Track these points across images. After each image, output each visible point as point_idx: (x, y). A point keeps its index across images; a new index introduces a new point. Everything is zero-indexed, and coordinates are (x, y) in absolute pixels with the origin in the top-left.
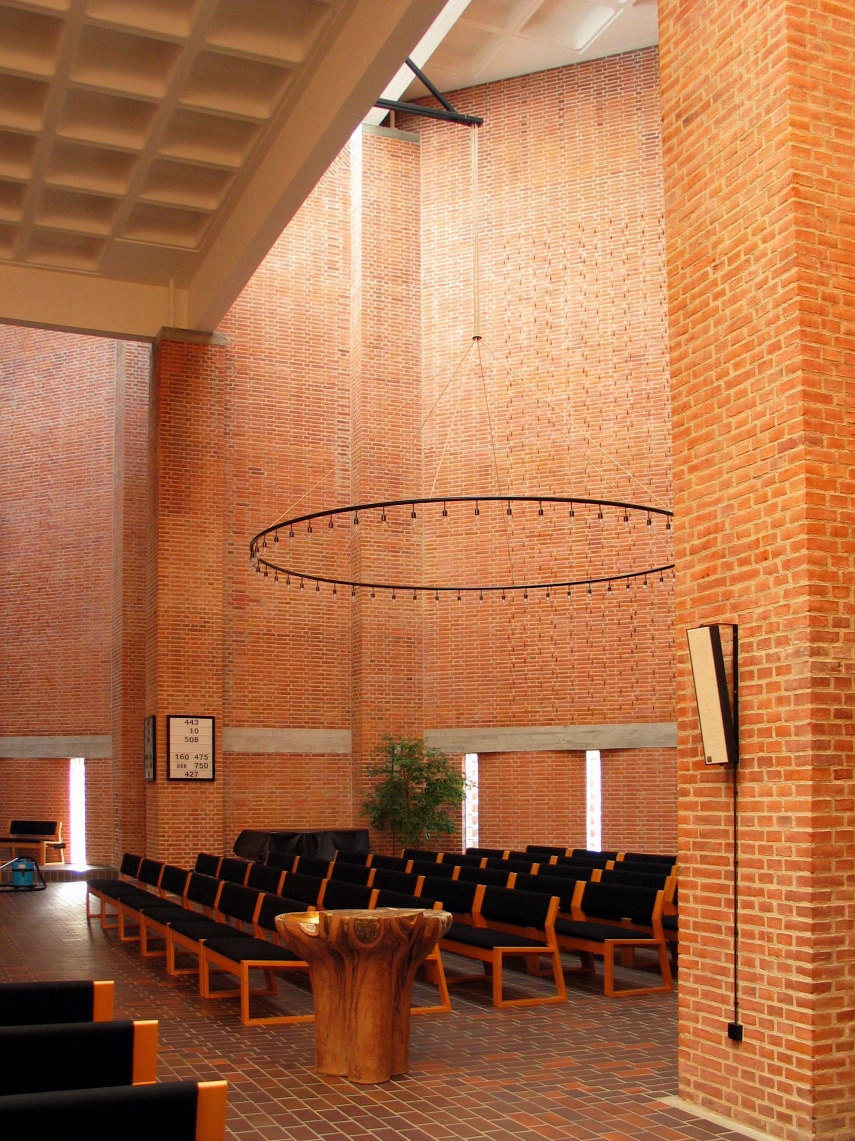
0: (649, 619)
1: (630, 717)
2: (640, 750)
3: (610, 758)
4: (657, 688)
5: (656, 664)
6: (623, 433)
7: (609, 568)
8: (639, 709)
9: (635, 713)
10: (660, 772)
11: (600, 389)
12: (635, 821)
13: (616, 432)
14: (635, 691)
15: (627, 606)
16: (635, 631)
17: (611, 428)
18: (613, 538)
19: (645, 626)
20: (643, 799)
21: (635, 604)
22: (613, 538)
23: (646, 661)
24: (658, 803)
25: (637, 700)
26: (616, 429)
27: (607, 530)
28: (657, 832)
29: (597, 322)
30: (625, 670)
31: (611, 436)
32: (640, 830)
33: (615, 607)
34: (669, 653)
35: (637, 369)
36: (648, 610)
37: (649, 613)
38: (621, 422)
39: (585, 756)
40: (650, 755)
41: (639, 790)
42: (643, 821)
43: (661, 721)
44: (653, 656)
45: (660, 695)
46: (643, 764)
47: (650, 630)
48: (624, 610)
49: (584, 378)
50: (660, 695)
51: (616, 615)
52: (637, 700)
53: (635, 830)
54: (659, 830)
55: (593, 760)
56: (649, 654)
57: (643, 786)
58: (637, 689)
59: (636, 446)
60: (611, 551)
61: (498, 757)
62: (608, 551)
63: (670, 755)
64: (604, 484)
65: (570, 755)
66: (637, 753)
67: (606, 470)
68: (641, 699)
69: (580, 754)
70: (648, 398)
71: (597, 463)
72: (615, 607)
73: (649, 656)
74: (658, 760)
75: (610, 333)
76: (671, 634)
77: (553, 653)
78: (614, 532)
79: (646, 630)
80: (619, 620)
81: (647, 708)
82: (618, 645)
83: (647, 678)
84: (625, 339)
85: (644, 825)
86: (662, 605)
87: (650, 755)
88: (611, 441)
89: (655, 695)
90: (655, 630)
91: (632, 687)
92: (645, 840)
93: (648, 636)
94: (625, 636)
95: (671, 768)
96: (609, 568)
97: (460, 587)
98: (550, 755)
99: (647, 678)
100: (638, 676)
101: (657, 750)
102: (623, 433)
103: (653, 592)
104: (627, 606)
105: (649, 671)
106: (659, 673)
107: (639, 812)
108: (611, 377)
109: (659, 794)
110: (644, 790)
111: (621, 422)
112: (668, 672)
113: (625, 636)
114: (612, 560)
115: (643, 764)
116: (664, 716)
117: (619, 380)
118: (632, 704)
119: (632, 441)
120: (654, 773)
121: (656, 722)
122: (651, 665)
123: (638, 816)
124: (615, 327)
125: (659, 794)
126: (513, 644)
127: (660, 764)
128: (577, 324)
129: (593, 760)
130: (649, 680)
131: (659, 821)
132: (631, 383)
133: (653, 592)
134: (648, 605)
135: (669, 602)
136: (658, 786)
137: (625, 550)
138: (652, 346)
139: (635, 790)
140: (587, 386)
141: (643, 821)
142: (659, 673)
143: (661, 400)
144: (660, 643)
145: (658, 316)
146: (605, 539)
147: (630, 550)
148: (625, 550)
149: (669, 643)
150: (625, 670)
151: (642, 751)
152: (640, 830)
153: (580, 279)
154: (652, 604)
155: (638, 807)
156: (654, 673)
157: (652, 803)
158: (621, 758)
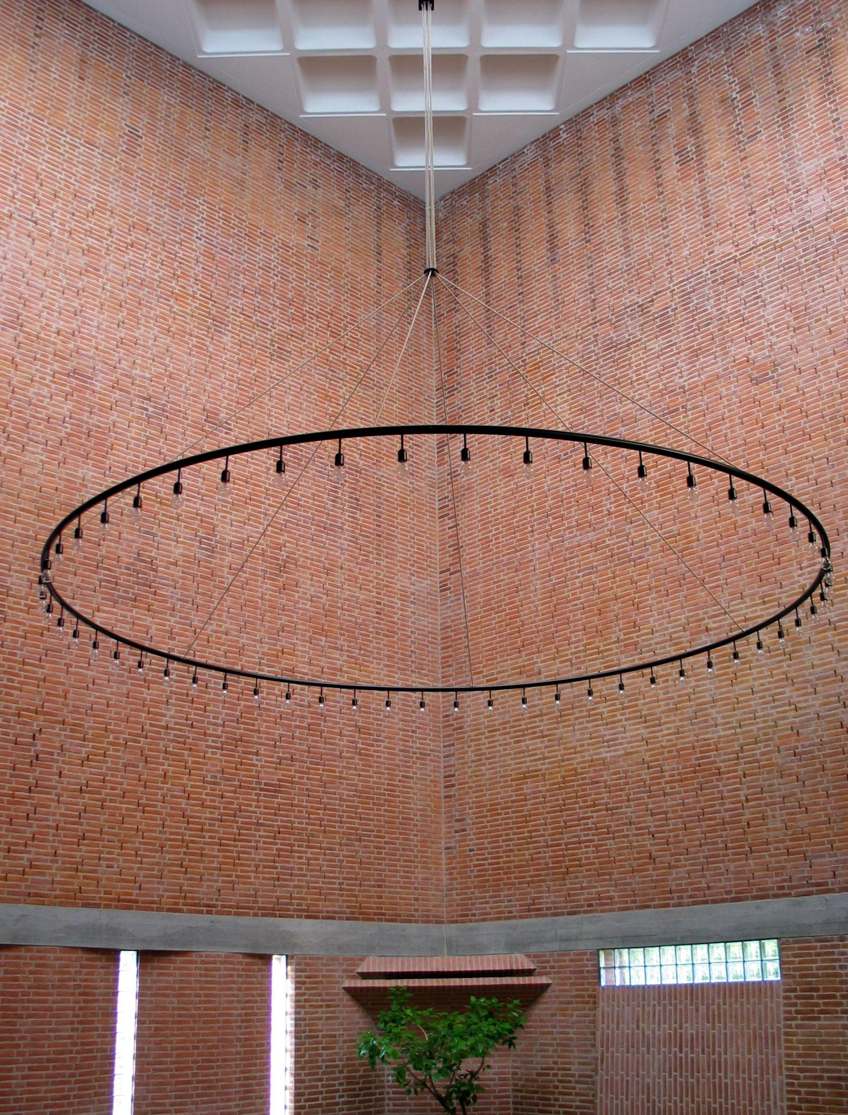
0: (58, 745)
1: (18, 894)
2: (28, 948)
3: (156, 964)
4: (60, 851)
5: (62, 815)
6: (52, 467)
7: (10, 654)
8: (33, 881)
9: (27, 887)
10: (53, 987)
11: (30, 394)
12: (10, 1070)
13: (43, 462)
14: (29, 852)
15: (30, 717)
16: (37, 758)
17: (36, 455)
18: (21, 611)
19: (52, 754)
20: (27, 1031)
21: (42, 718)
22: (21, 611)
23: (49, 807)
24: (48, 1038)
25: (31, 866)
26: (43, 458)
27: (14, 596)
28: (44, 1088)
29: (40, 307)
30: (18, 817)
31: (36, 465)
32: (17, 1086)
33: (13, 715)
34: (81, 801)
35: (80, 391)
36: (57, 731)
37: (58, 735)
38: (51, 452)
39: (117, 960)
40: (41, 958)
41: (21, 1017)
42: (23, 1069)
43: (61, 904)
44: (58, 802)
45: (63, 863)
46: (31, 972)
47: (57, 761)
48: (25, 724)
49: (13, 371)
50: (63, 863)
51: (14, 728)
52: (31, 866)
53: (9, 1086)
54: (46, 1084)
55: (128, 962)
56: (53, 797)
57: (27, 1009)
58: (33, 850)
59: (66, 492)
60: (17, 629)
61: (173, 958)
62: (13, 628)
63: (70, 959)
64: (18, 528)
65: (103, 957)
66: (23, 953)
67: (22, 510)
68: (37, 867)
69: (113, 956)
70: (89, 435)
71: (12, 495)
72: (13, 715)
73: (52, 800)
74: (53, 966)
75: (54, 329)
76: (84, 772)
77: (185, 786)
78: (23, 602)
79: (52, 760)
80: (17, 736)
81: (44, 882)
82: (12, 776)
83: (47, 834)
84: (71, 346)
85: (23, 1078)
86: (76, 727)
87: (41, 958)
88: (35, 471)
89: (57, 862)
90: (64, 762)
91: (26, 845)
92: (24, 1104)
93: (55, 770)
94: (23, 763)
95: (69, 980)
96: (10, 654)
97: (559, 678)
98: (80, 954)
99: (47, 834)
100: (35, 829)
101: (52, 950)
102: (52, 467)
103: (67, 705)
104: (30, 717)
105: (51, 823)
106: (64, 829)
107: (20, 1054)
108: (47, 385)
109: (50, 1023)
110: (29, 1016)
111: (51, 452)
112: (76, 830)
113: (23, 763)
114: (16, 642)
115: (31, 972)
116: (67, 897)
117: (57, 395)
118: (24, 873)
119: (63, 482)
120: (46, 987)
121: (55, 905)
122: (54, 814)
123: (17, 1062)
124: (61, 325)
125: (50, 1023)
126: (39, 748)
127: (55, 973)
128: (14, 295)
129: (128, 962)
130: (51, 838)
131: (47, 1068)
132: (69, 406)
133: (67, 705)
134: (58, 722)
135: (87, 724)
136: (50, 1009)
137: (36, 633)
138: (102, 372)
139: (16, 1016)
140: (14, 382)
141: (23, 1069)
142: (64, 829)
143: (104, 445)
144: (69, 783)
145: (115, 339)
146: (10, 608)
147: (42, 635)
148: (36, 633)
149: (81, 785)
150: (18, 817)
151: (31, 951)
152: (17, 1086)
153: (28, 242)
154: (64, 723)
155: (18, 1046)
156: (57, 828)
157: (39, 1039)
158: (172, 965)
